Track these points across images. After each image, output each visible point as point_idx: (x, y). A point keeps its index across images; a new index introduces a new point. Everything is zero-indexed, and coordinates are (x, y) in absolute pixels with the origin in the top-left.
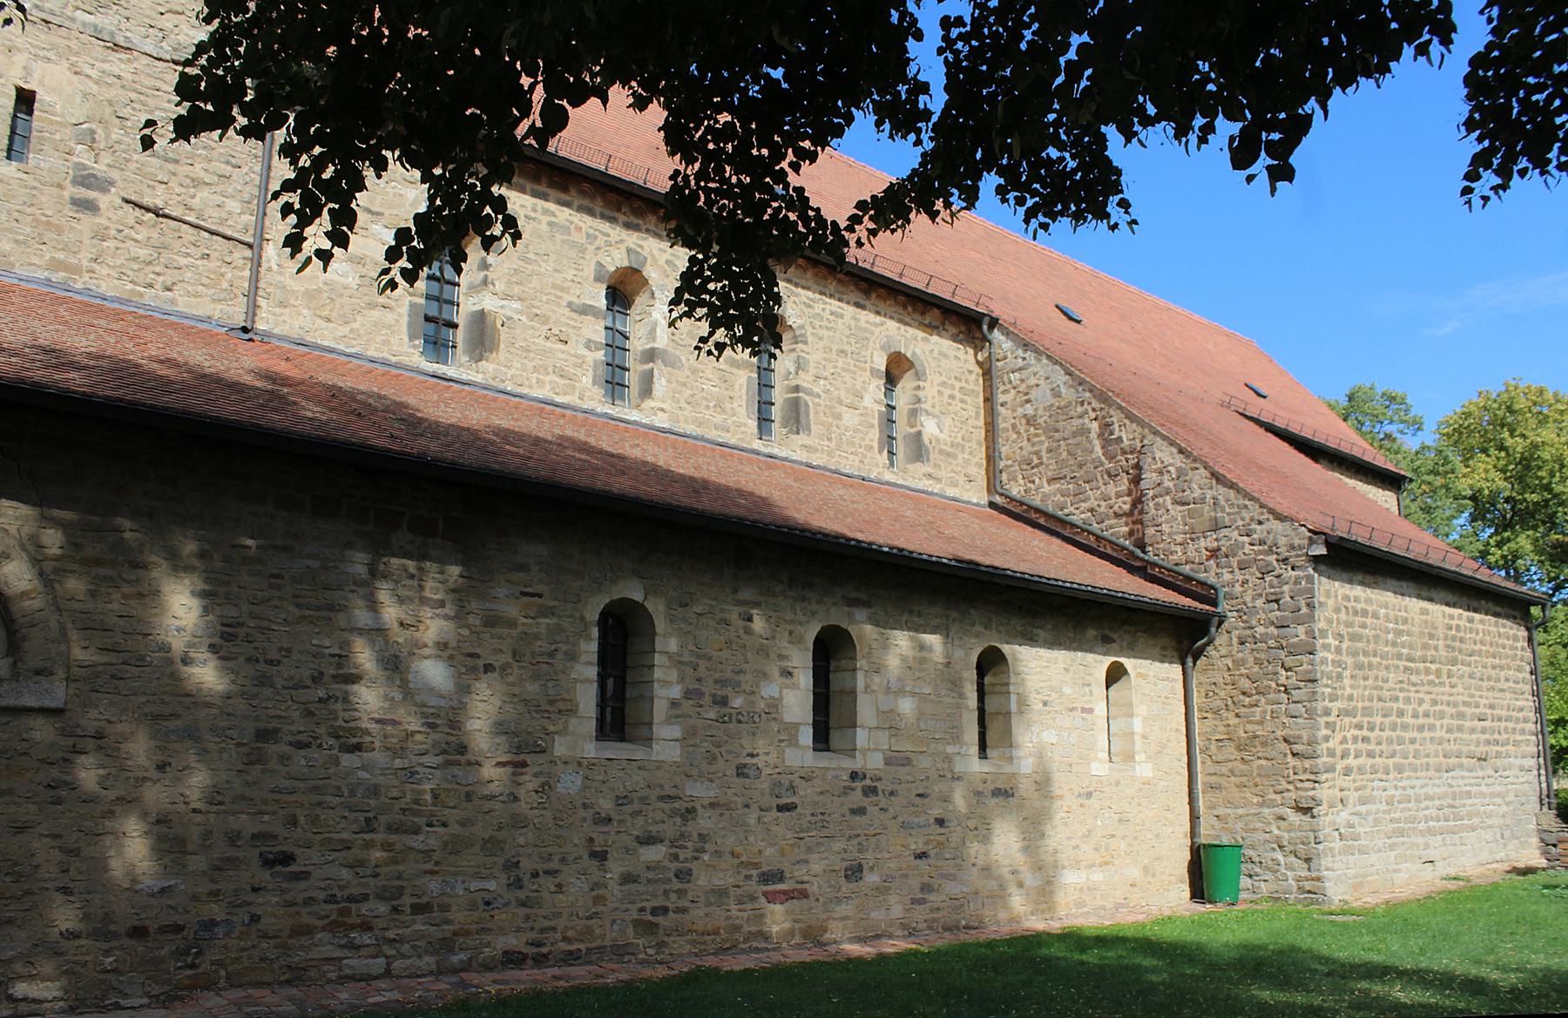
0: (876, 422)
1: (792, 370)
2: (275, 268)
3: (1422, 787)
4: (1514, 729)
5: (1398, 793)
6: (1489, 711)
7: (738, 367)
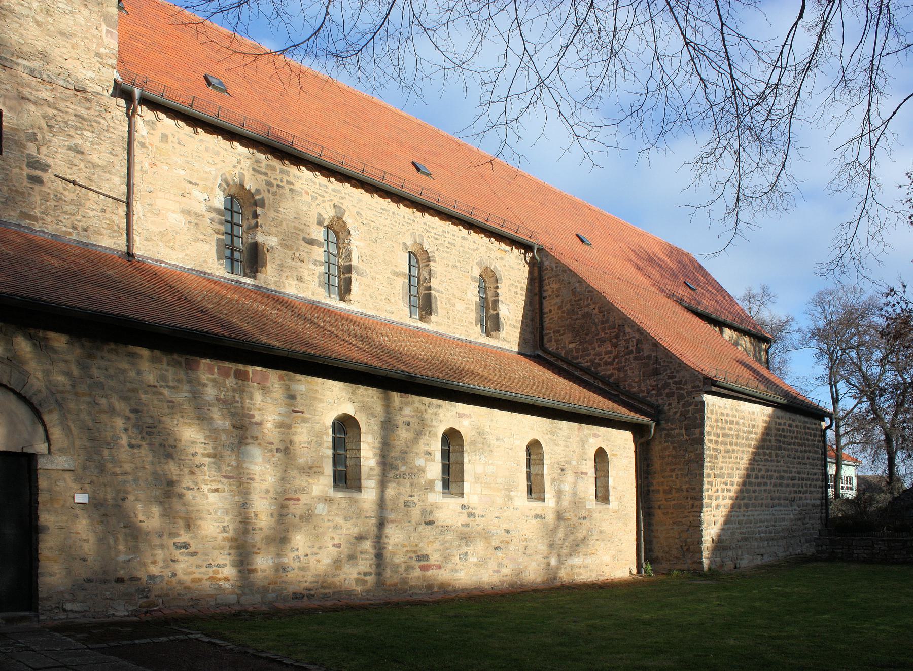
0: (474, 308)
1: (428, 277)
3: (759, 515)
4: (811, 485)
5: (746, 518)
6: (797, 475)
7: (397, 276)
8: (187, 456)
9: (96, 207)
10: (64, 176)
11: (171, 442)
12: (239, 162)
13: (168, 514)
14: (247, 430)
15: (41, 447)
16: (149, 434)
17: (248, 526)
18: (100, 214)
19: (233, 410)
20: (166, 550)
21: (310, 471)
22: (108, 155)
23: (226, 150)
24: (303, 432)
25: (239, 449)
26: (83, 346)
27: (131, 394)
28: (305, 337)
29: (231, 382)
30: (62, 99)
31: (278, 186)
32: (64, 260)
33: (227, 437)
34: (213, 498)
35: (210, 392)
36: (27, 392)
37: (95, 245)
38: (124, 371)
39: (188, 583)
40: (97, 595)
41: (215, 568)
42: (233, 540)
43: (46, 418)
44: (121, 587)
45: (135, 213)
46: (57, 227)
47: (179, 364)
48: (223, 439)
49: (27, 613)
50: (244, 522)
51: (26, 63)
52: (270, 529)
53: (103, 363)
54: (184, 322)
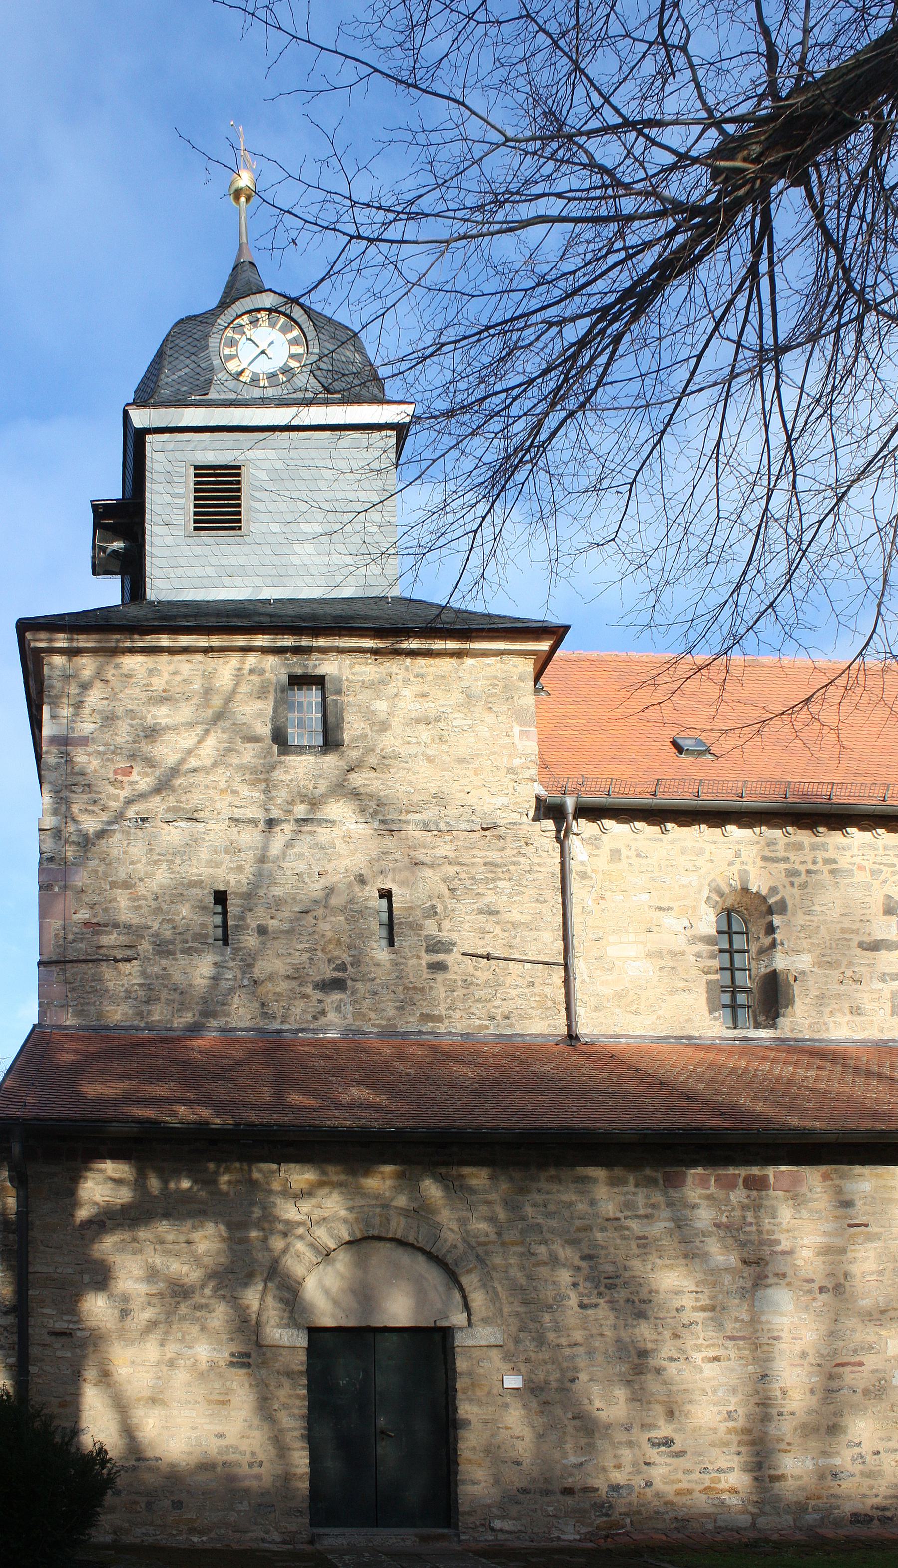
2: (587, 979)
8: (668, 1312)
9: (520, 981)
10: (475, 952)
11: (644, 1294)
12: (738, 854)
13: (639, 1398)
14: (767, 1264)
15: (459, 1319)
16: (609, 1287)
17: (770, 1410)
18: (527, 990)
19: (742, 1237)
20: (636, 1448)
21: (882, 1317)
22: (534, 905)
23: (715, 843)
24: (868, 1257)
25: (753, 1295)
26: (511, 1179)
27: (581, 1235)
28: (868, 1103)
29: (738, 1195)
30: (467, 848)
31: (808, 872)
32: (478, 1065)
33: (734, 1279)
34: (710, 1370)
35: (704, 1216)
36: (440, 1249)
37: (522, 1035)
38: (570, 1205)
39: (671, 1497)
40: (535, 1510)
41: (714, 1474)
42: (746, 1431)
43: (465, 1280)
44: (569, 1500)
45: (577, 976)
46: (469, 1022)
47: (653, 1182)
48: (726, 1283)
49: (445, 1531)
50: (763, 1404)
51: (417, 817)
52: (809, 1413)
53: (539, 1198)
54: (659, 1120)
